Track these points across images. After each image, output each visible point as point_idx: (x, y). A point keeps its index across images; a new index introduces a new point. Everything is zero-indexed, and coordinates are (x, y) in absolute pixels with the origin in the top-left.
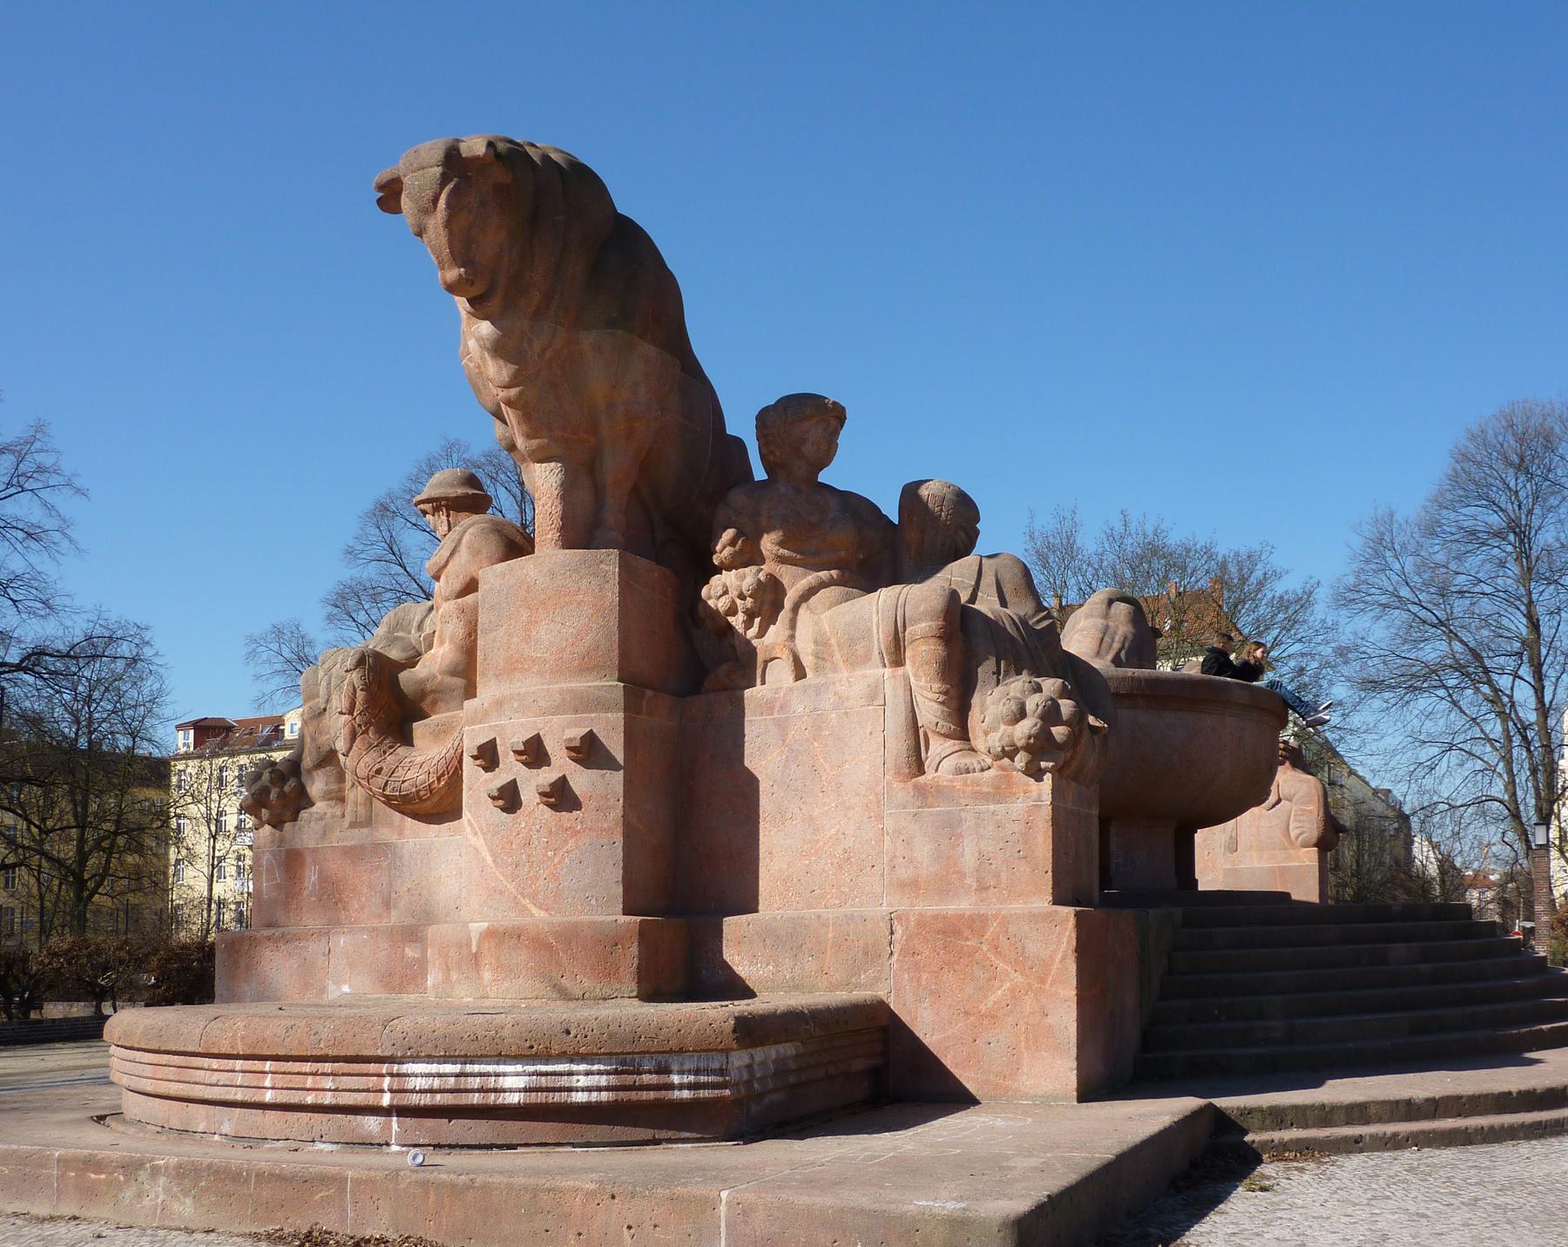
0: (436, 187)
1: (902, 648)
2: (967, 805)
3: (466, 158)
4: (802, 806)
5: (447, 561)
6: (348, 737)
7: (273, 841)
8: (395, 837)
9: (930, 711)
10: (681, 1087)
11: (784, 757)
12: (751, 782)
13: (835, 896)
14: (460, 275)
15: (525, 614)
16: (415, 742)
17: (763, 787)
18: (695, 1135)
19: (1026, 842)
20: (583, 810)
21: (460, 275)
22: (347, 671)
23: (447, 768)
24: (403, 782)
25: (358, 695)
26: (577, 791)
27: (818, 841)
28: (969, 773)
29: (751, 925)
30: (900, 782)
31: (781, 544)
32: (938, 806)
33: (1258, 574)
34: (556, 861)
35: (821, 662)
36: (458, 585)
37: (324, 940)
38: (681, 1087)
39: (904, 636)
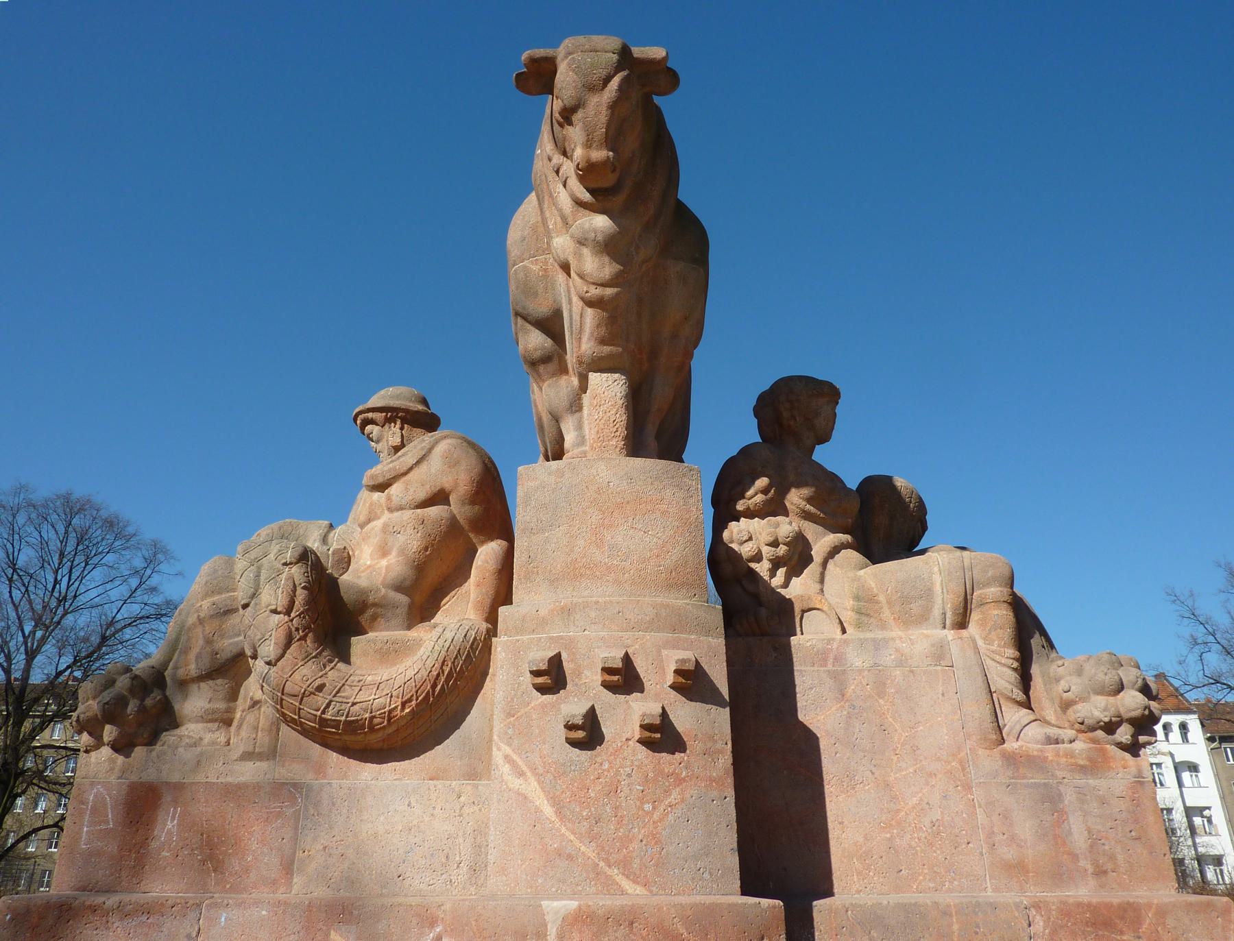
0: (610, 70)
1: (969, 610)
2: (1064, 778)
3: (637, 58)
4: (874, 770)
5: (411, 469)
6: (282, 640)
7: (112, 769)
8: (311, 775)
9: (1004, 678)
11: (845, 713)
12: (808, 742)
13: (928, 877)
14: (608, 157)
15: (595, 517)
16: (353, 659)
17: (823, 744)
19: (1136, 821)
20: (688, 751)
21: (608, 157)
22: (285, 564)
23: (417, 692)
24: (354, 704)
25: (297, 593)
26: (680, 728)
27: (898, 811)
28: (1058, 743)
29: (850, 912)
30: (986, 748)
31: (809, 500)
32: (1032, 778)
34: (656, 817)
35: (864, 618)
36: (422, 495)
37: (192, 915)
39: (972, 598)
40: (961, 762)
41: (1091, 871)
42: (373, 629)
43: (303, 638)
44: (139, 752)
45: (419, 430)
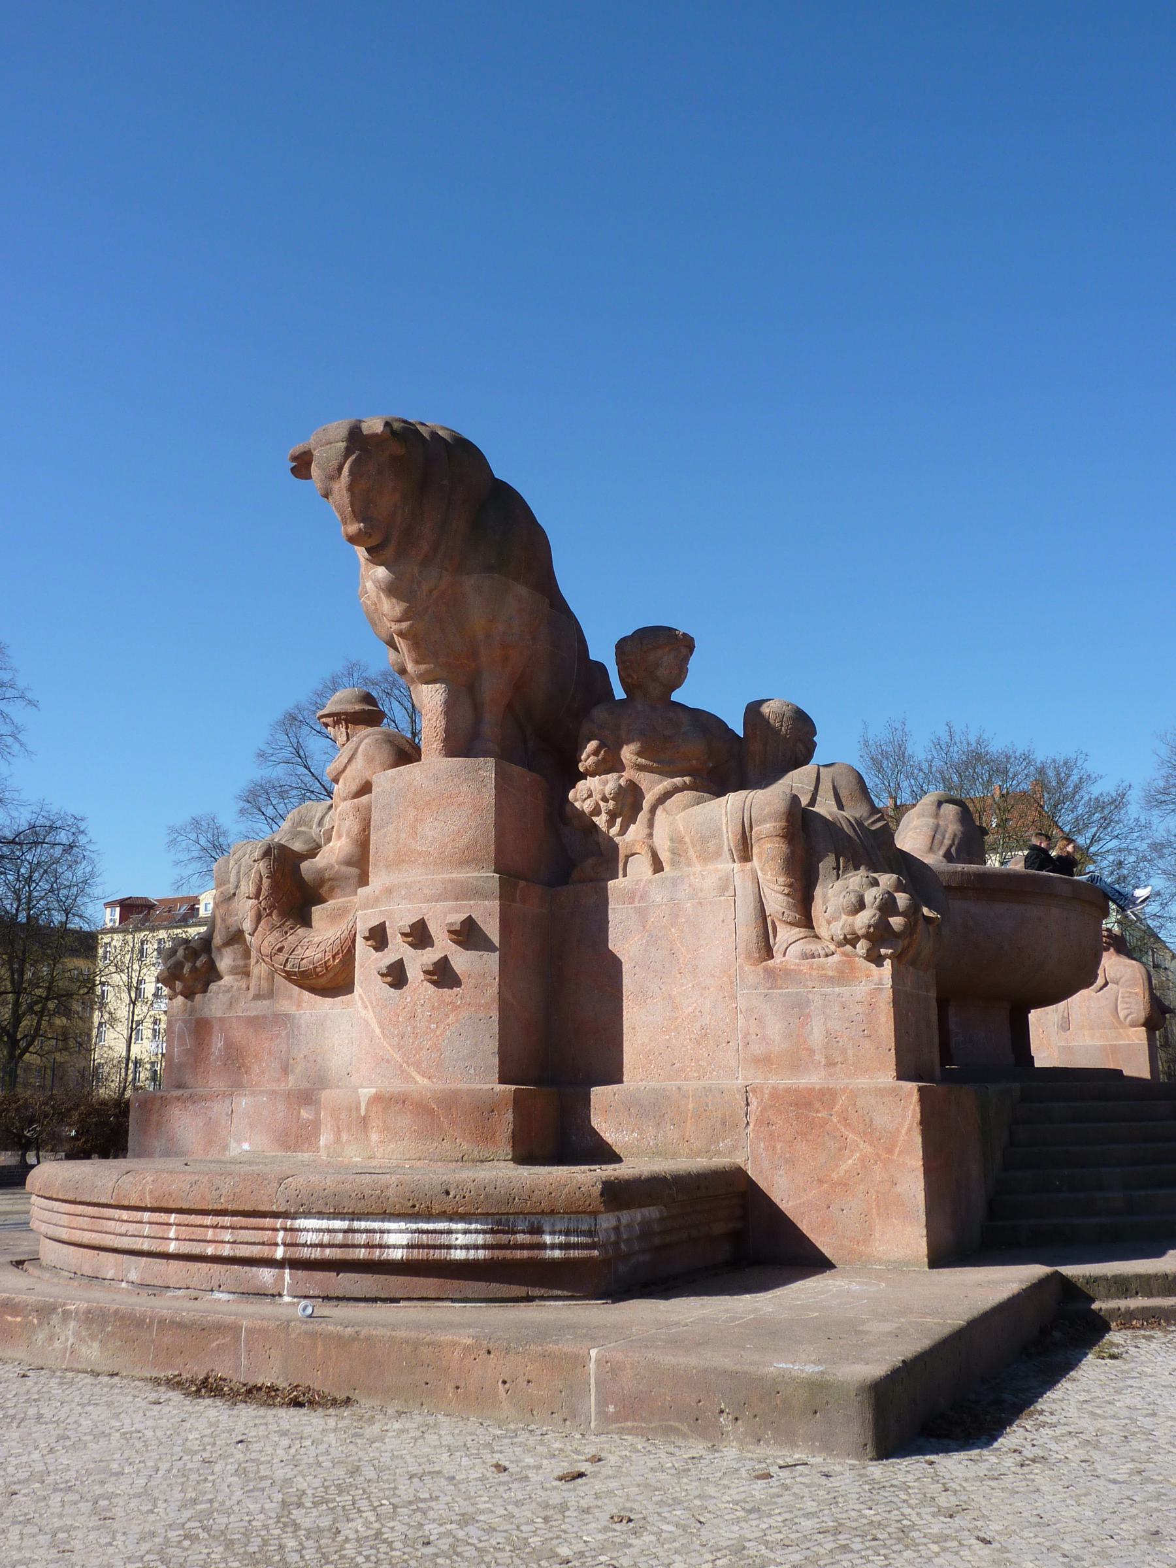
3: (367, 435)
4: (662, 986)
5: (346, 767)
6: (254, 918)
8: (294, 1008)
10: (553, 1247)
18: (566, 1293)
22: (255, 861)
24: (302, 959)
31: (639, 754)
33: (1075, 778)
34: (438, 1033)
35: (677, 858)
36: (354, 788)
38: (553, 1247)
40: (730, 976)
41: (823, 1063)
42: (332, 898)
43: (270, 915)
44: (198, 997)
45: (360, 727)
